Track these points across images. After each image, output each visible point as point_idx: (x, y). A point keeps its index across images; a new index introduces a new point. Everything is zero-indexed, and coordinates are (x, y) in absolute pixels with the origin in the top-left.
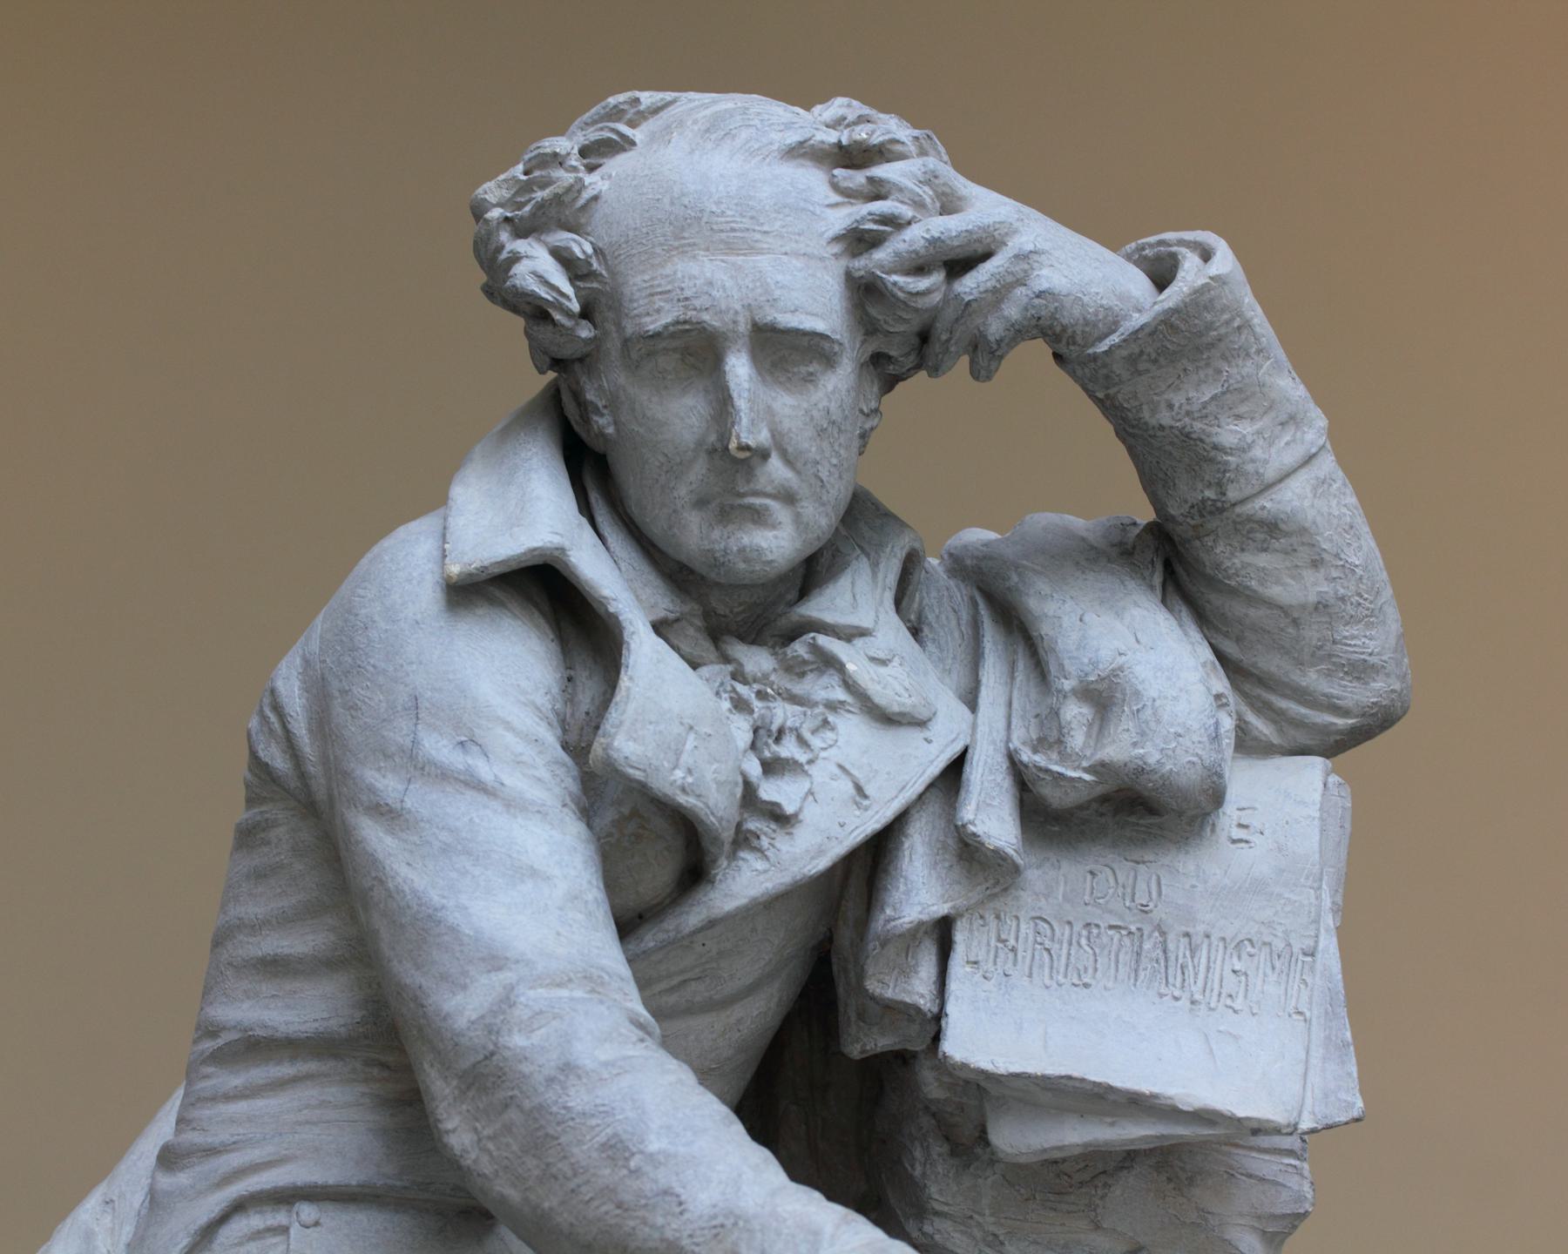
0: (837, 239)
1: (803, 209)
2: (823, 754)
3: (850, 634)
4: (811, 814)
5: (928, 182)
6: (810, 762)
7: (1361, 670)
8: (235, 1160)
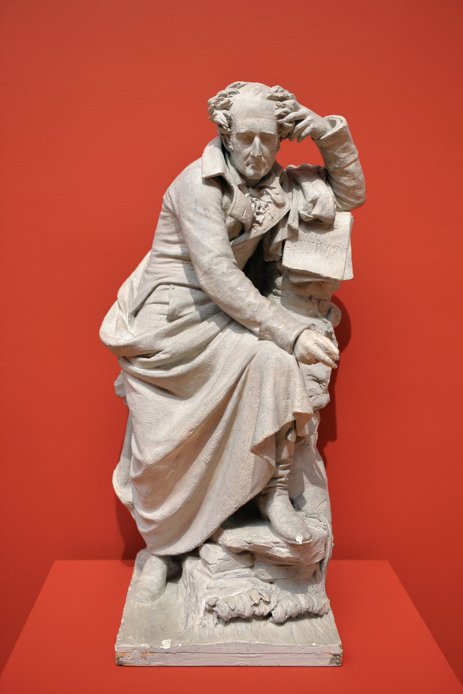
0: (276, 116)
1: (271, 110)
2: (267, 211)
3: (271, 188)
4: (265, 222)
5: (293, 105)
6: (264, 213)
7: (358, 198)
8: (160, 276)
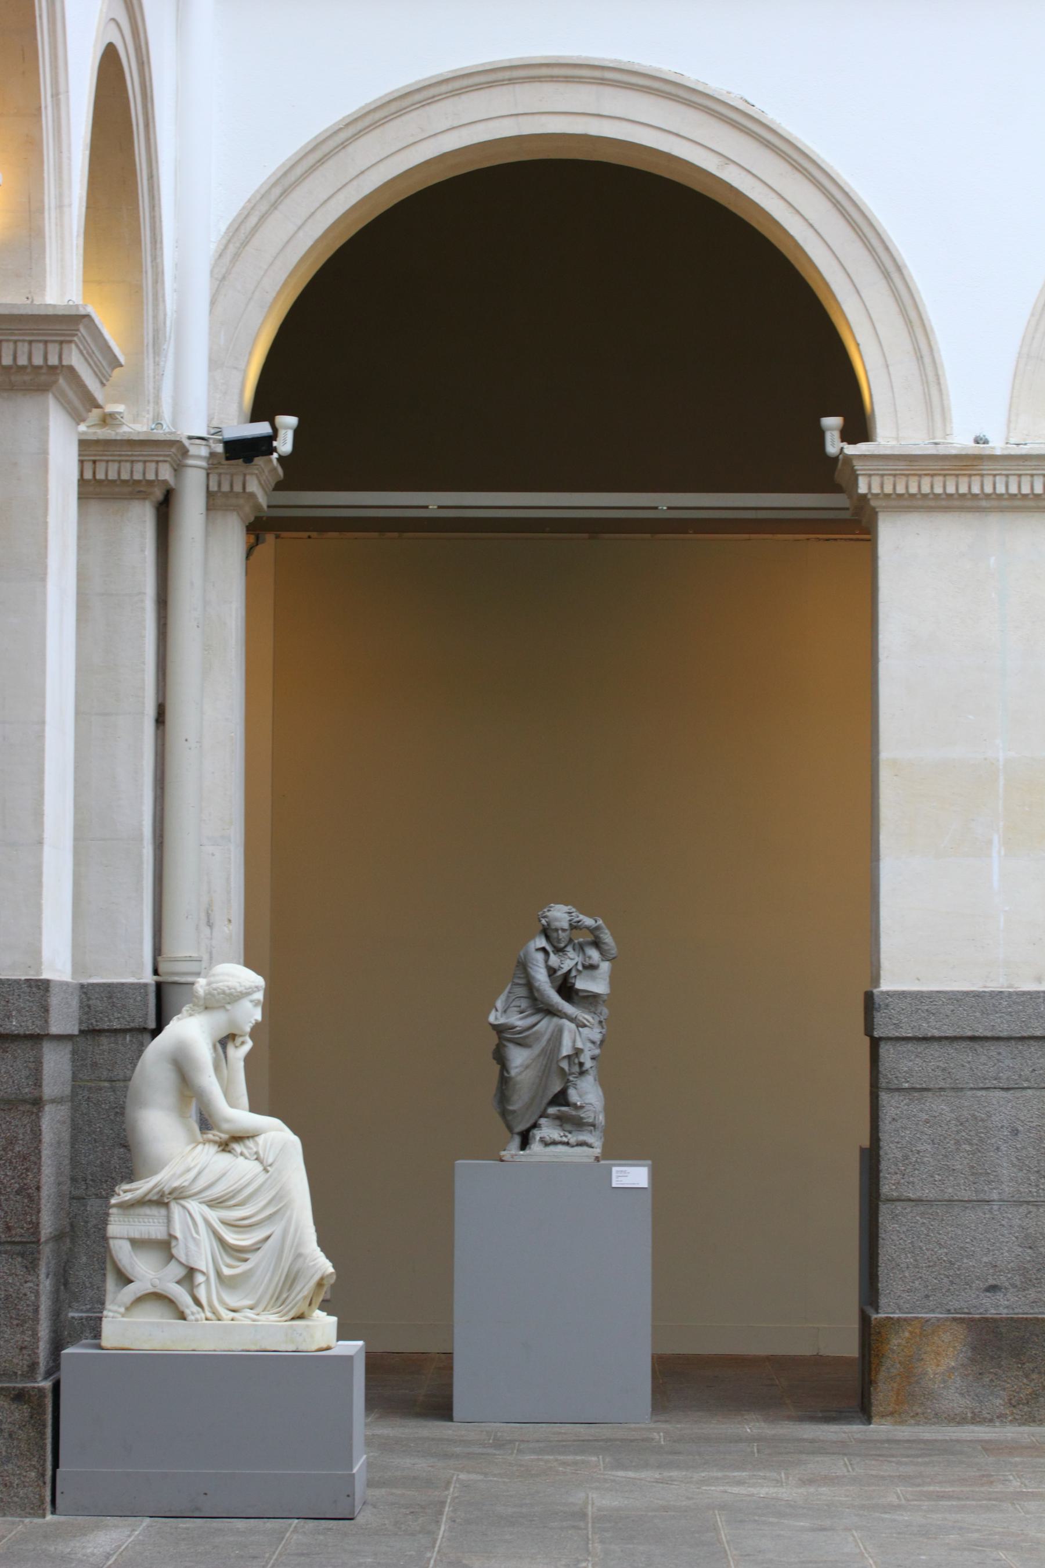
7: (613, 954)
